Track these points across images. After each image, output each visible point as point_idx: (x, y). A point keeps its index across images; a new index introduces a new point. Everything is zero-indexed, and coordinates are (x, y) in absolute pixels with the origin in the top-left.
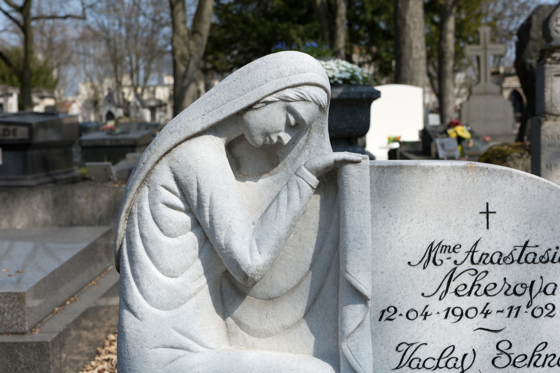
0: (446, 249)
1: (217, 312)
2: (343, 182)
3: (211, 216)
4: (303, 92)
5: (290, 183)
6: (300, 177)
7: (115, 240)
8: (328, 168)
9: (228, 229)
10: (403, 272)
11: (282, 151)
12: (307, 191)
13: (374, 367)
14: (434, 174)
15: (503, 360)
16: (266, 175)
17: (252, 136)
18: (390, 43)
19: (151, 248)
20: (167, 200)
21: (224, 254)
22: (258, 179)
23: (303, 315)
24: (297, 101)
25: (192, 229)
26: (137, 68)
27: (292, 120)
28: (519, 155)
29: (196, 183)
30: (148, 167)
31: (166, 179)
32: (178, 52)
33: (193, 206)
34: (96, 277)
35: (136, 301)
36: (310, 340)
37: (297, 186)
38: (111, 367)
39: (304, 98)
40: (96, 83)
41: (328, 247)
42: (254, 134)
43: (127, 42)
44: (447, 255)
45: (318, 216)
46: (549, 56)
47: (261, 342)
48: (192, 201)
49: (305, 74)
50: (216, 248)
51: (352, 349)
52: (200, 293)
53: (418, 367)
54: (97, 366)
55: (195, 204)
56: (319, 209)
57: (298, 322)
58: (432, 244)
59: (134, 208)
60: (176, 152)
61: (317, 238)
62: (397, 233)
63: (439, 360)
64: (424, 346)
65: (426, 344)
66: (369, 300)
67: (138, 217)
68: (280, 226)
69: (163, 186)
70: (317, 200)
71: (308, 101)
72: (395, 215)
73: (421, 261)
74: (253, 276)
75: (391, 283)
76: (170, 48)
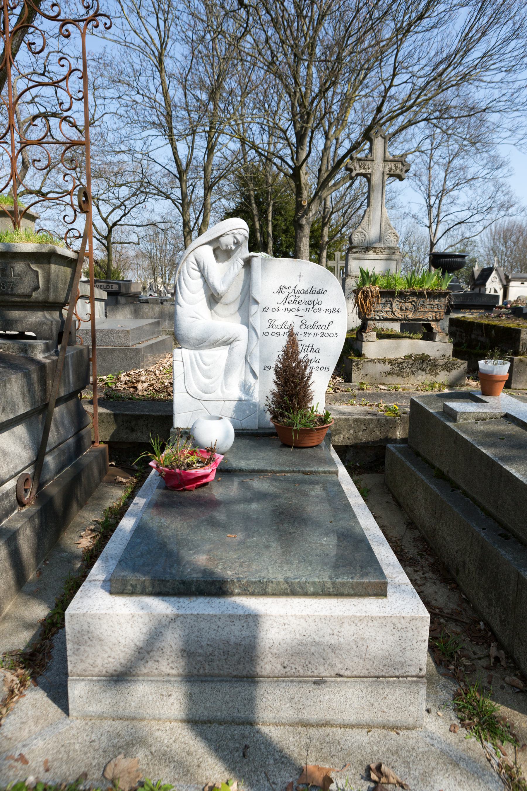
0: (286, 288)
15: (304, 326)
26: (165, 273)
27: (236, 241)
36: (240, 319)
41: (247, 287)
70: (243, 270)
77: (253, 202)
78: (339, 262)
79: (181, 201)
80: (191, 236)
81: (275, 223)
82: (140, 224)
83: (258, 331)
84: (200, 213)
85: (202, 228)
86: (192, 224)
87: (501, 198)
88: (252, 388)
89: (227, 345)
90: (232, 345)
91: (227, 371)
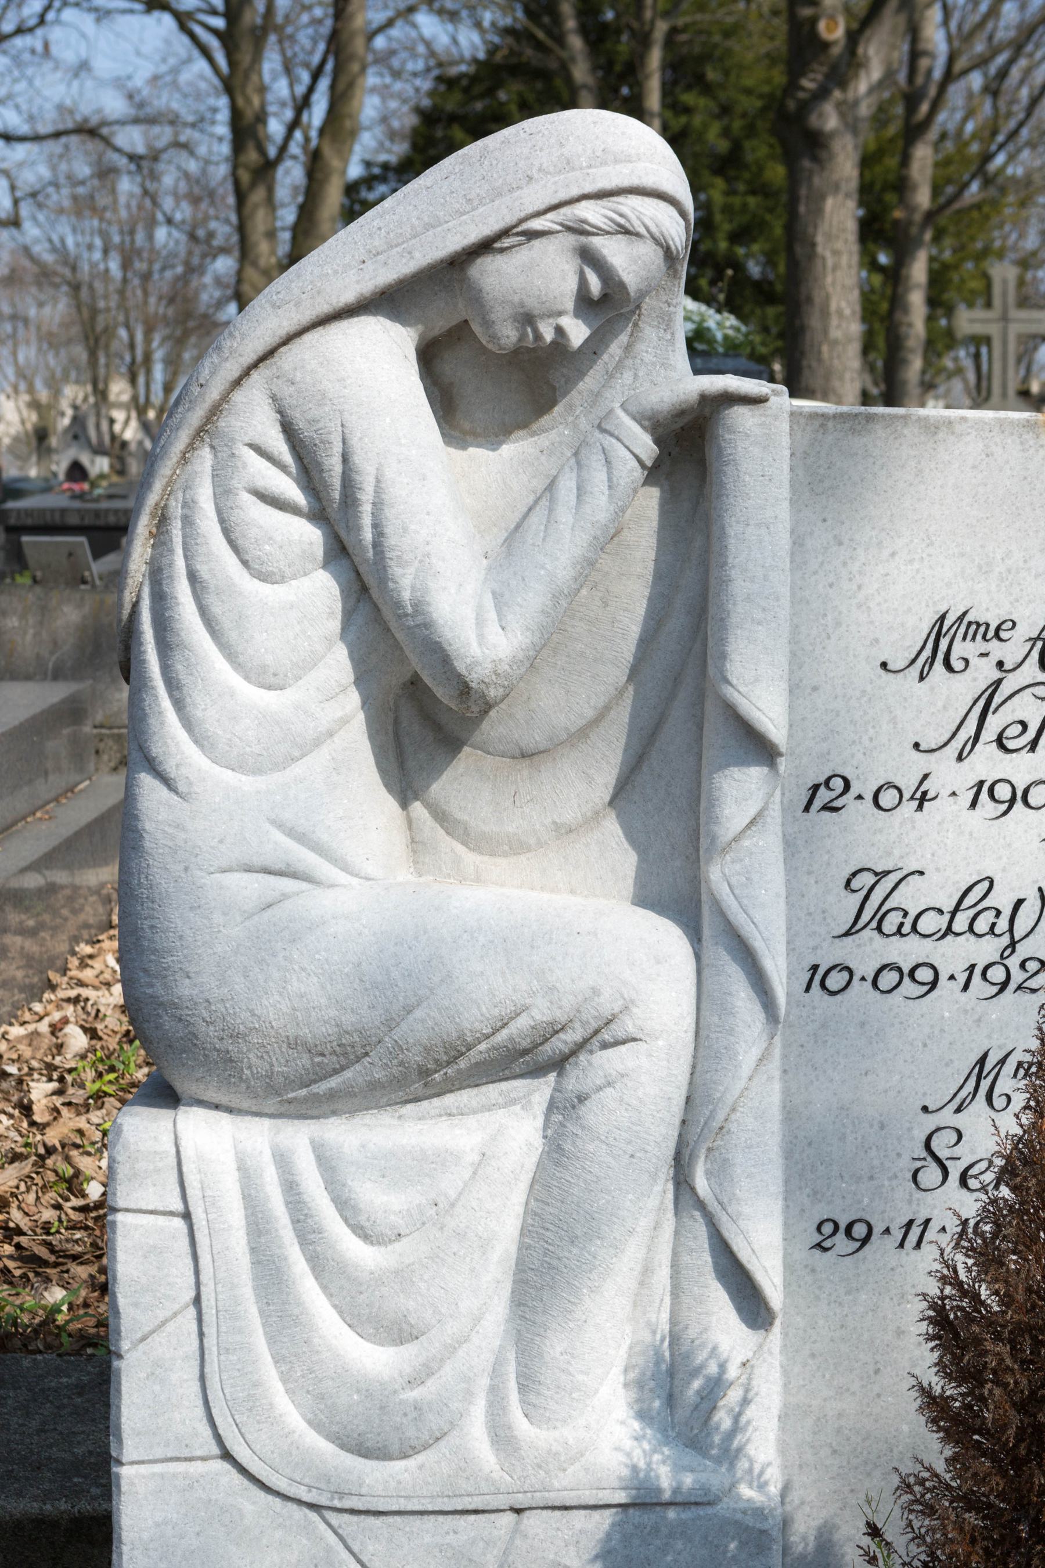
0: (977, 630)
1: (386, 786)
2: (720, 450)
3: (376, 526)
5: (583, 451)
6: (612, 435)
7: (121, 591)
8: (681, 413)
9: (421, 562)
10: (869, 688)
11: (565, 371)
12: (629, 471)
13: (788, 929)
14: (952, 438)
16: (521, 433)
17: (487, 324)
18: (771, 311)
19: (216, 608)
20: (261, 484)
21: (409, 628)
22: (500, 444)
23: (608, 798)
24: (608, 233)
26: (148, 359)
29: (340, 439)
30: (214, 393)
31: (259, 427)
33: (330, 500)
34: (48, 803)
35: (173, 750)
36: (627, 861)
38: (84, 1017)
39: (627, 225)
40: (43, 395)
41: (677, 623)
43: (122, 293)
44: (980, 646)
45: (653, 542)
47: (497, 867)
48: (327, 486)
49: (630, 166)
50: (387, 613)
51: (734, 881)
52: (342, 732)
53: (899, 932)
54: (47, 1015)
55: (336, 495)
56: (655, 524)
57: (596, 816)
58: (942, 618)
59: (172, 503)
60: (289, 358)
62: (855, 587)
63: (953, 914)
64: (916, 877)
65: (922, 873)
66: (780, 755)
67: (183, 528)
68: (557, 559)
69: (251, 446)
71: (638, 235)
72: (851, 540)
73: (913, 661)
74: (483, 686)
75: (838, 715)
77: (571, 24)
78: (1014, 313)
79: (219, 23)
80: (270, 191)
82: (24, 129)
83: (777, 967)
84: (316, 75)
85: (327, 151)
86: (275, 128)
88: (734, 1396)
89: (537, 1071)
90: (573, 1082)
91: (542, 1278)
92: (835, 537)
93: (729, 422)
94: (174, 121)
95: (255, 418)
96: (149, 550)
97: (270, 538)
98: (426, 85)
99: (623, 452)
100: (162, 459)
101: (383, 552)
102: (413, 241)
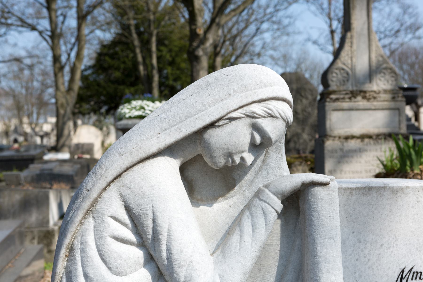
2: (310, 206)
3: (168, 250)
4: (270, 107)
6: (265, 202)
8: (295, 190)
9: (188, 265)
11: (239, 172)
14: (403, 195)
16: (221, 199)
17: (212, 157)
24: (264, 117)
25: (145, 265)
26: (32, 113)
27: (258, 139)
28: (299, 163)
29: (152, 213)
30: (94, 195)
32: (60, 102)
33: (147, 239)
37: (262, 212)
39: (272, 113)
40: (7, 121)
42: (215, 154)
45: (279, 243)
46: (328, 97)
48: (145, 233)
55: (150, 237)
56: (279, 235)
58: (403, 271)
59: (76, 242)
60: (127, 177)
61: (278, 267)
62: (367, 260)
67: (81, 253)
69: (111, 217)
71: (276, 117)
76: (53, 101)
81: (160, 54)
87: (409, 21)
92: (358, 239)
93: (314, 194)
94: (38, 56)
95: (113, 204)
96: (65, 263)
97: (121, 257)
98: (98, 47)
99: (271, 209)
100: (71, 223)
101: (172, 261)
102: (181, 124)
